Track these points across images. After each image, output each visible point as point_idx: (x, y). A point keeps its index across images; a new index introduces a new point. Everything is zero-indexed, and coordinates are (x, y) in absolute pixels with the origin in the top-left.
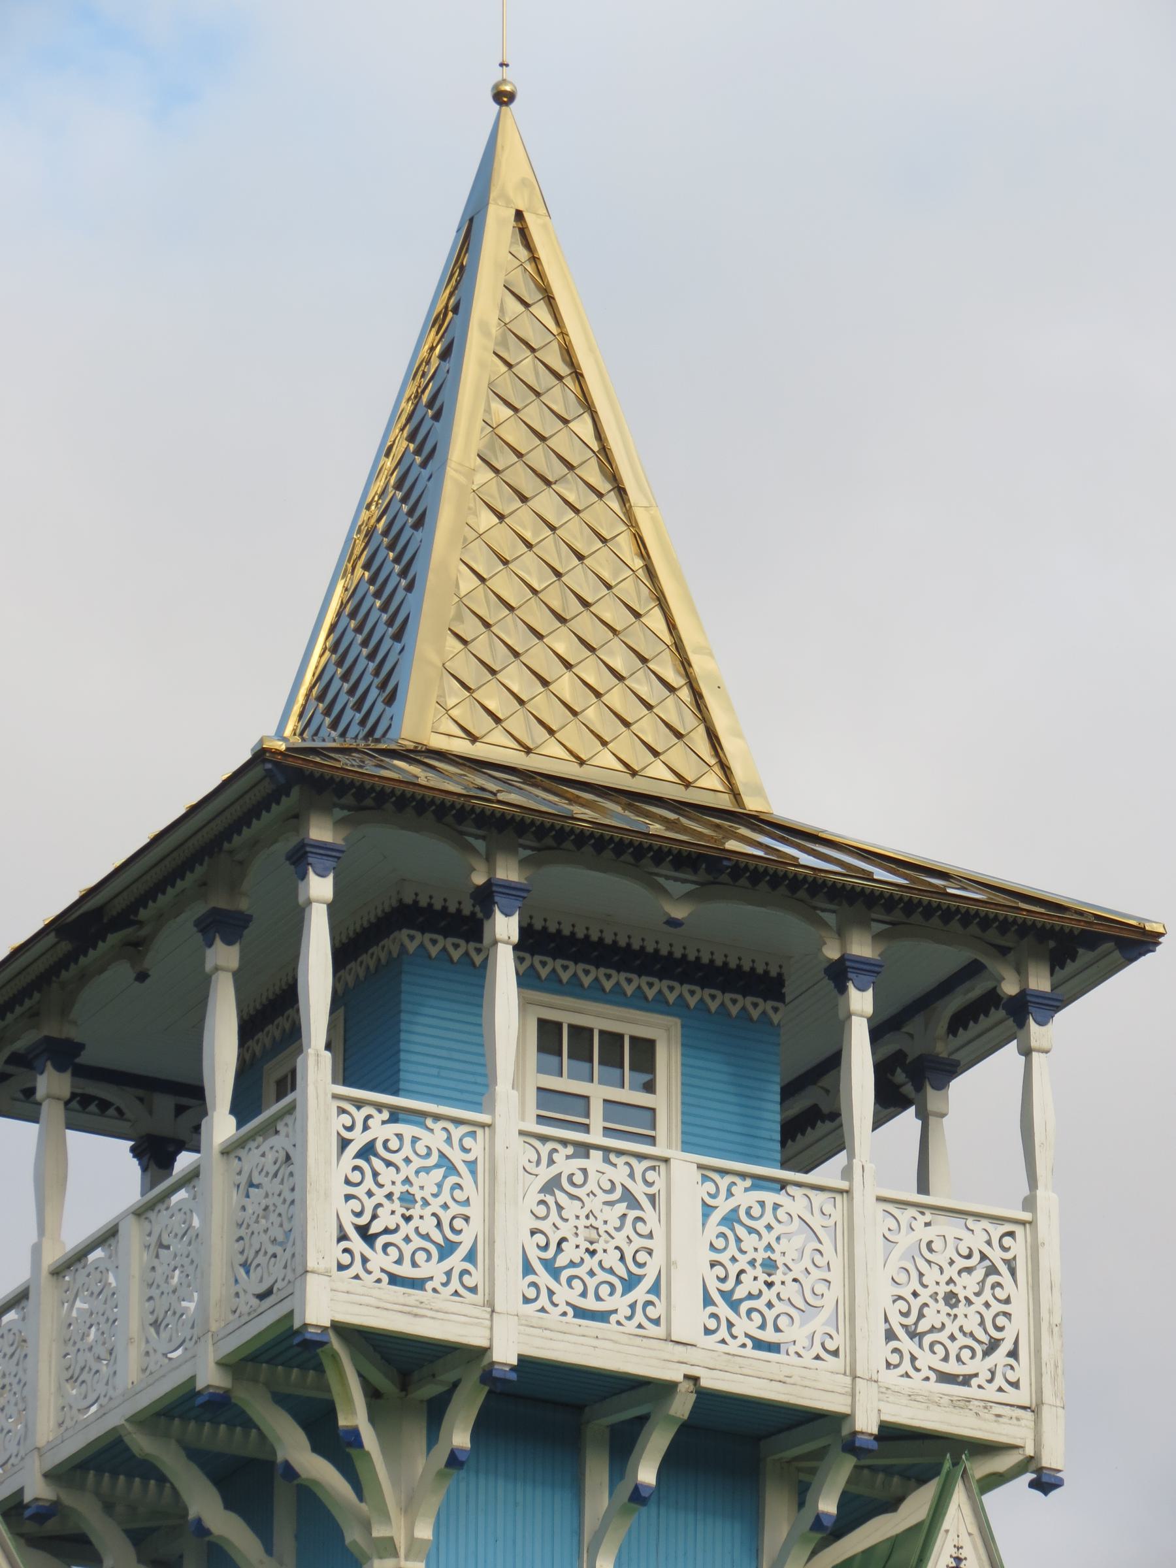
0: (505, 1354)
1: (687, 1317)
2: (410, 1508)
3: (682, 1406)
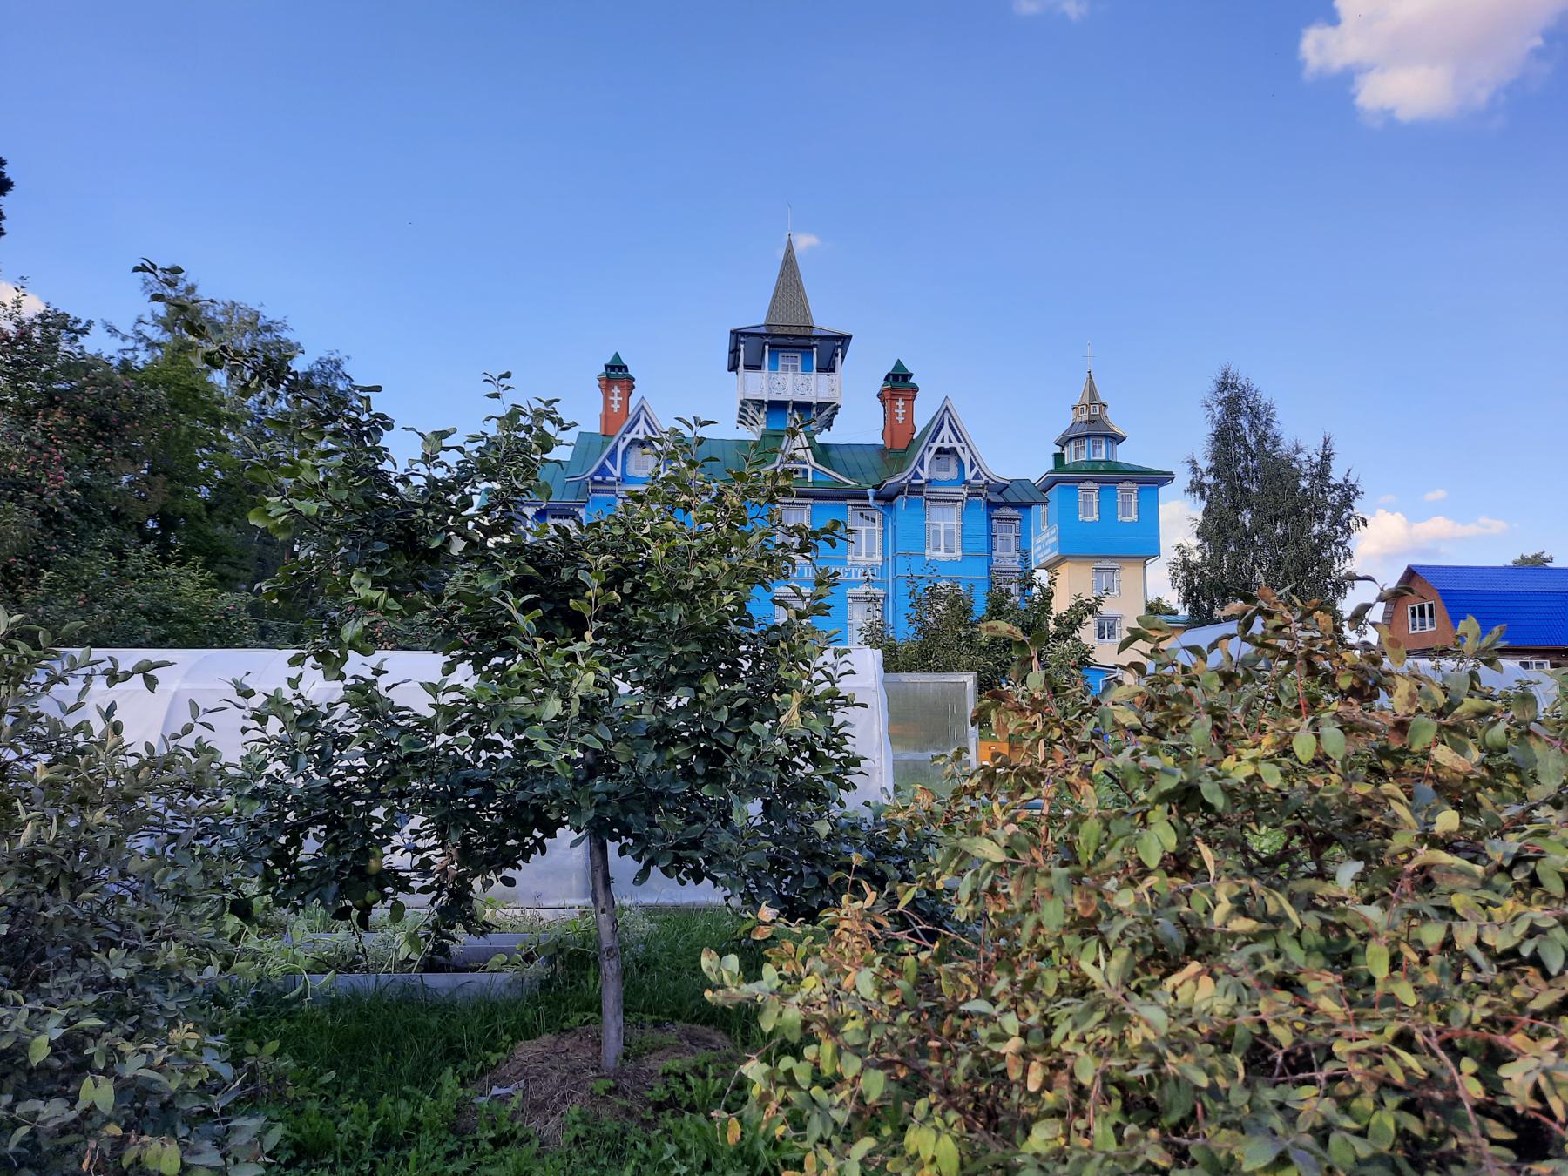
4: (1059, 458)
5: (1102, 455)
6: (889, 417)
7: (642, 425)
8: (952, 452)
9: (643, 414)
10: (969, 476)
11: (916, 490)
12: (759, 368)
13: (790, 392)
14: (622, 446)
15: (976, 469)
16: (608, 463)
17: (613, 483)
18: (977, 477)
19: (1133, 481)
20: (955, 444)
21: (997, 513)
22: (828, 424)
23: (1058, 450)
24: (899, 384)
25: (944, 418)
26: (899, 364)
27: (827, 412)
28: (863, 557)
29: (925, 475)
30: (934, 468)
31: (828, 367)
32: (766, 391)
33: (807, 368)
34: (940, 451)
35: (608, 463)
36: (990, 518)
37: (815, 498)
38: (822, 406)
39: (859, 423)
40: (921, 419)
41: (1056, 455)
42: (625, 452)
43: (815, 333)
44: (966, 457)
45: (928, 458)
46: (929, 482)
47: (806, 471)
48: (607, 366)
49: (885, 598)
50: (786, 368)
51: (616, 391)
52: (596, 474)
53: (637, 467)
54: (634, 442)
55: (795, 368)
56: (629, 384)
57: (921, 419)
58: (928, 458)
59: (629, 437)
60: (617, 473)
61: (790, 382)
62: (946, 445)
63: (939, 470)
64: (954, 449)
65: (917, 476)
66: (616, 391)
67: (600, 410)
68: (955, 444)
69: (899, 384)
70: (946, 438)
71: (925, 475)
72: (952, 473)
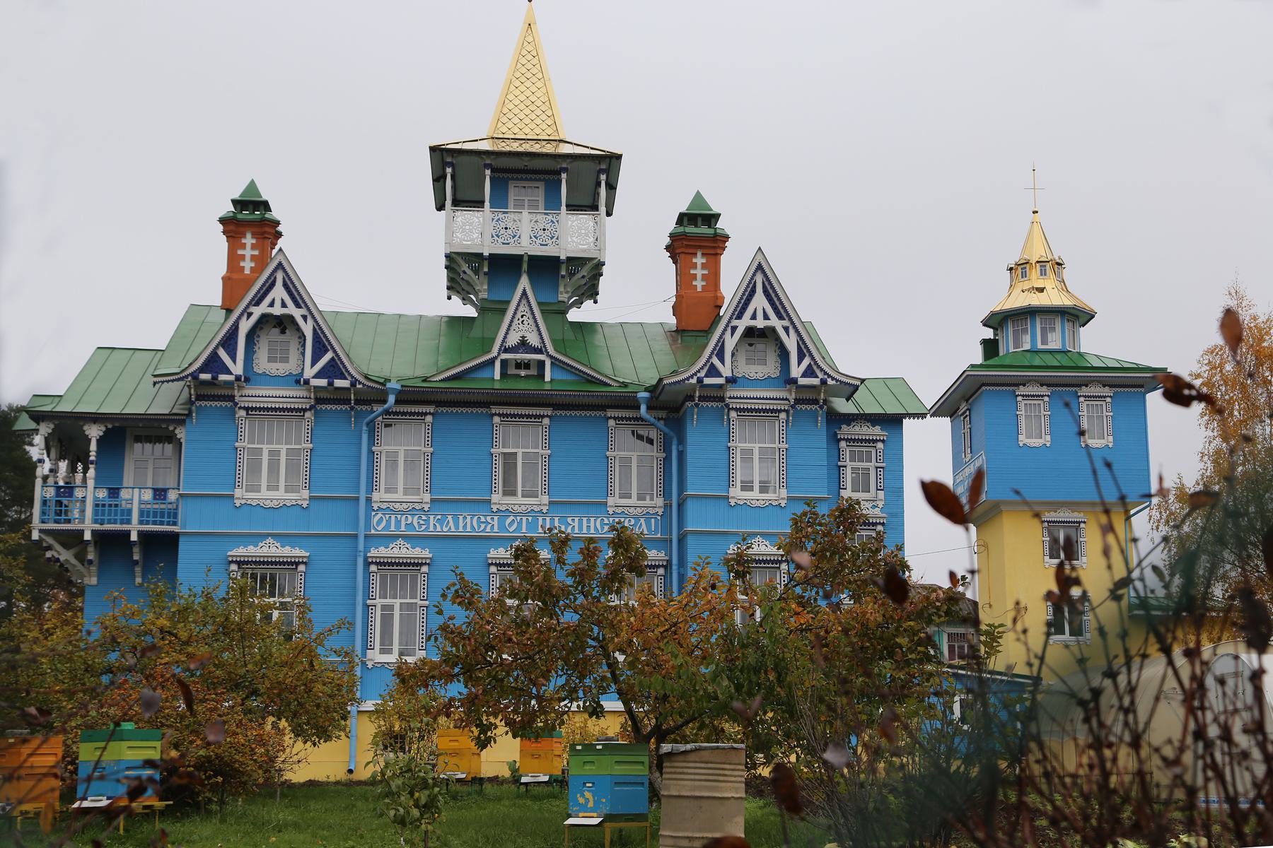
0: (486, 254)
1: (525, 241)
2: (482, 284)
3: (526, 259)
4: (990, 347)
5: (1054, 342)
6: (683, 279)
7: (278, 292)
8: (767, 334)
9: (280, 276)
10: (796, 371)
11: (716, 396)
12: (479, 204)
13: (525, 241)
14: (245, 326)
15: (806, 361)
16: (222, 354)
17: (228, 384)
18: (809, 372)
19: (1105, 384)
20: (774, 322)
21: (846, 431)
22: (591, 291)
23: (989, 334)
24: (696, 236)
25: (761, 279)
26: (252, 186)
27: (584, 272)
28: (633, 501)
29: (726, 371)
30: (741, 358)
31: (586, 204)
32: (488, 239)
33: (552, 203)
34: (750, 332)
35: (222, 354)
36: (835, 440)
37: (439, 404)
38: (575, 262)
39: (635, 295)
40: (731, 281)
41: (985, 343)
42: (251, 335)
43: (565, 149)
44: (791, 343)
45: (730, 343)
46: (732, 380)
47: (541, 364)
48: (235, 202)
49: (668, 566)
50: (519, 205)
51: (249, 240)
52: (203, 369)
53: (271, 360)
54: (265, 319)
55: (533, 205)
56: (268, 231)
57: (731, 281)
58: (730, 343)
59: (257, 312)
60: (238, 369)
61: (525, 228)
62: (760, 323)
63: (749, 361)
64: (773, 330)
65: (713, 372)
66: (249, 240)
67: (222, 269)
68: (774, 322)
69: (696, 236)
70: (760, 313)
71: (726, 371)
72: (770, 368)
